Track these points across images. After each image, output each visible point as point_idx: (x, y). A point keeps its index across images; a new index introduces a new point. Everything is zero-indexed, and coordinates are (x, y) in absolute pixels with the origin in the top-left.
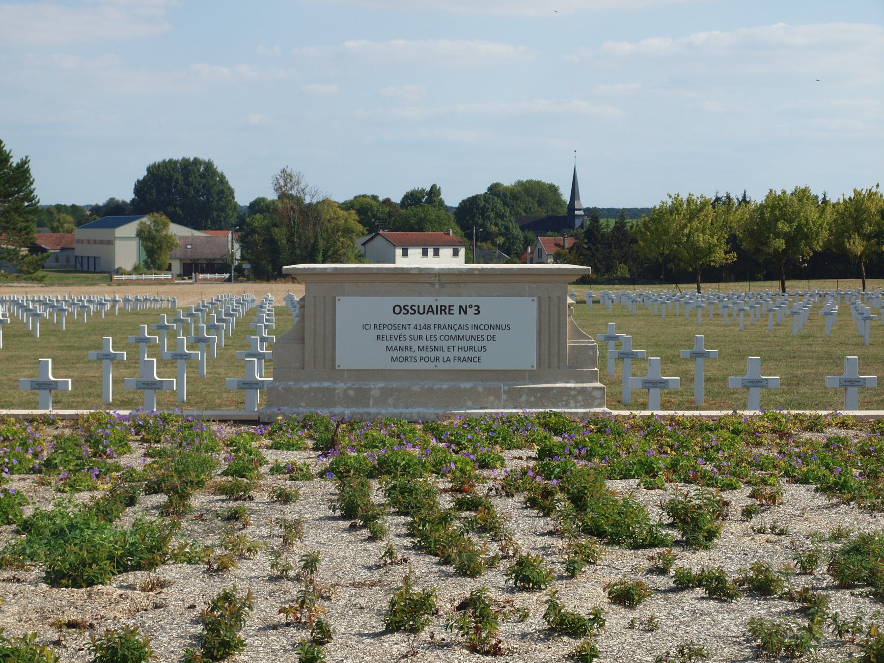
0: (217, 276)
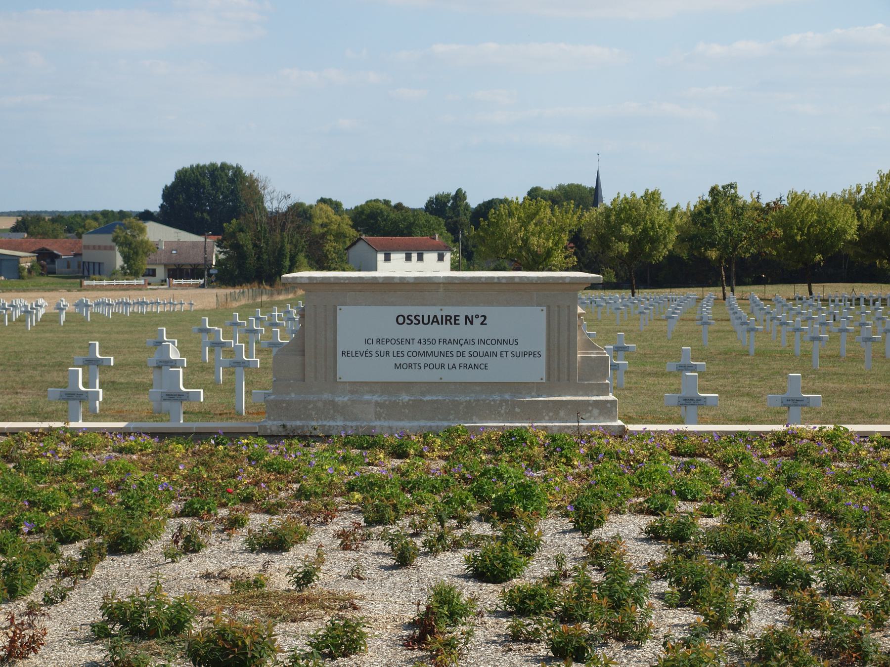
0: (191, 281)
